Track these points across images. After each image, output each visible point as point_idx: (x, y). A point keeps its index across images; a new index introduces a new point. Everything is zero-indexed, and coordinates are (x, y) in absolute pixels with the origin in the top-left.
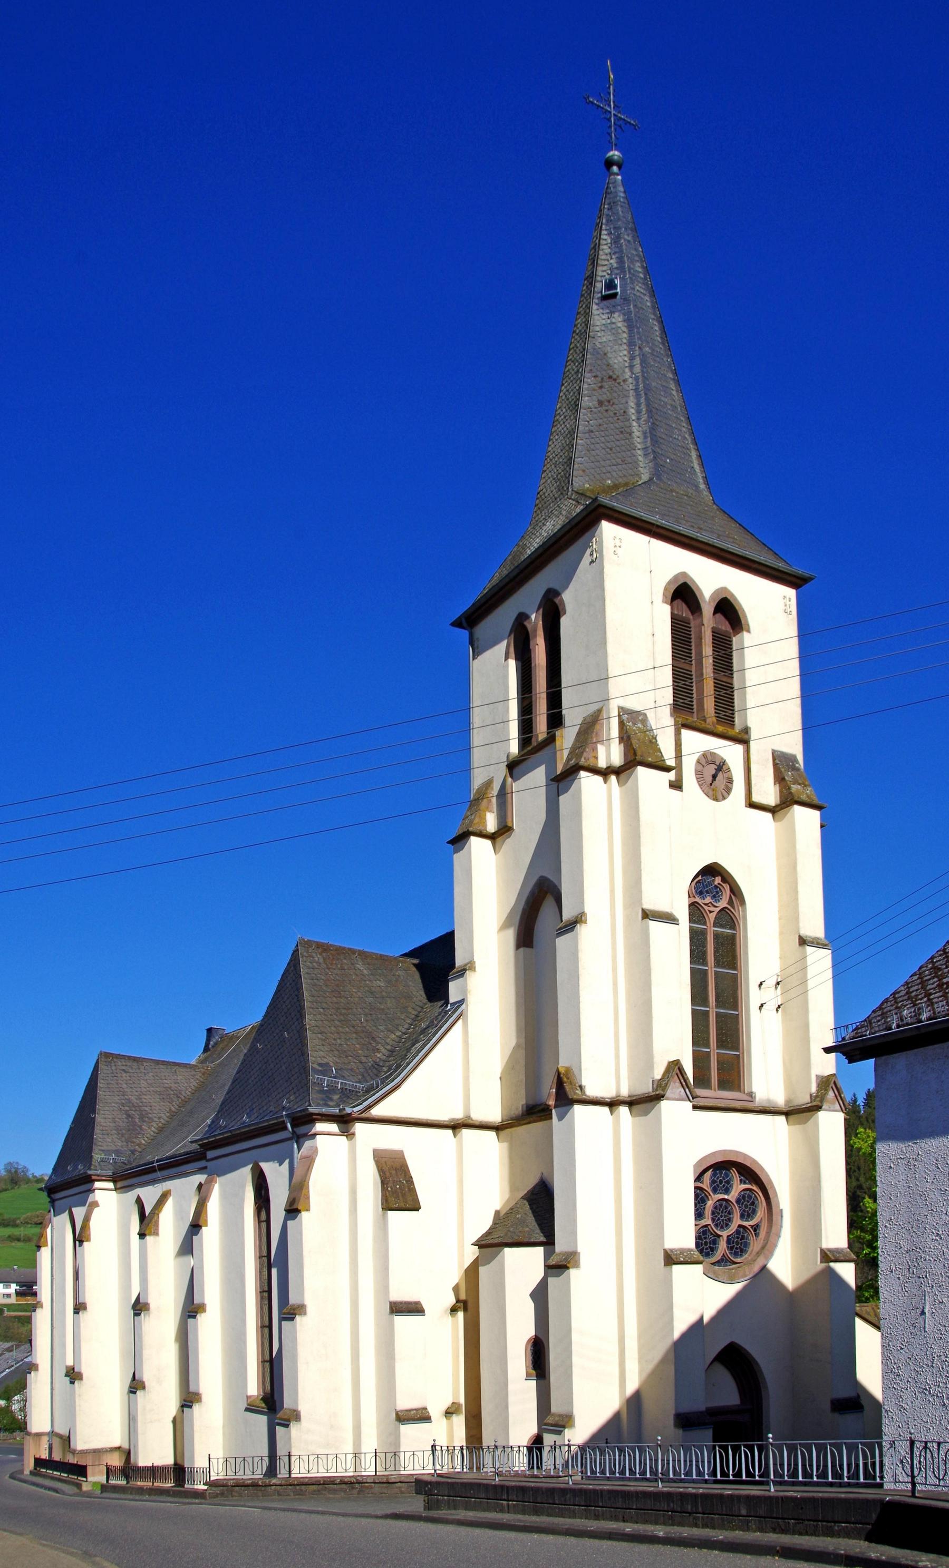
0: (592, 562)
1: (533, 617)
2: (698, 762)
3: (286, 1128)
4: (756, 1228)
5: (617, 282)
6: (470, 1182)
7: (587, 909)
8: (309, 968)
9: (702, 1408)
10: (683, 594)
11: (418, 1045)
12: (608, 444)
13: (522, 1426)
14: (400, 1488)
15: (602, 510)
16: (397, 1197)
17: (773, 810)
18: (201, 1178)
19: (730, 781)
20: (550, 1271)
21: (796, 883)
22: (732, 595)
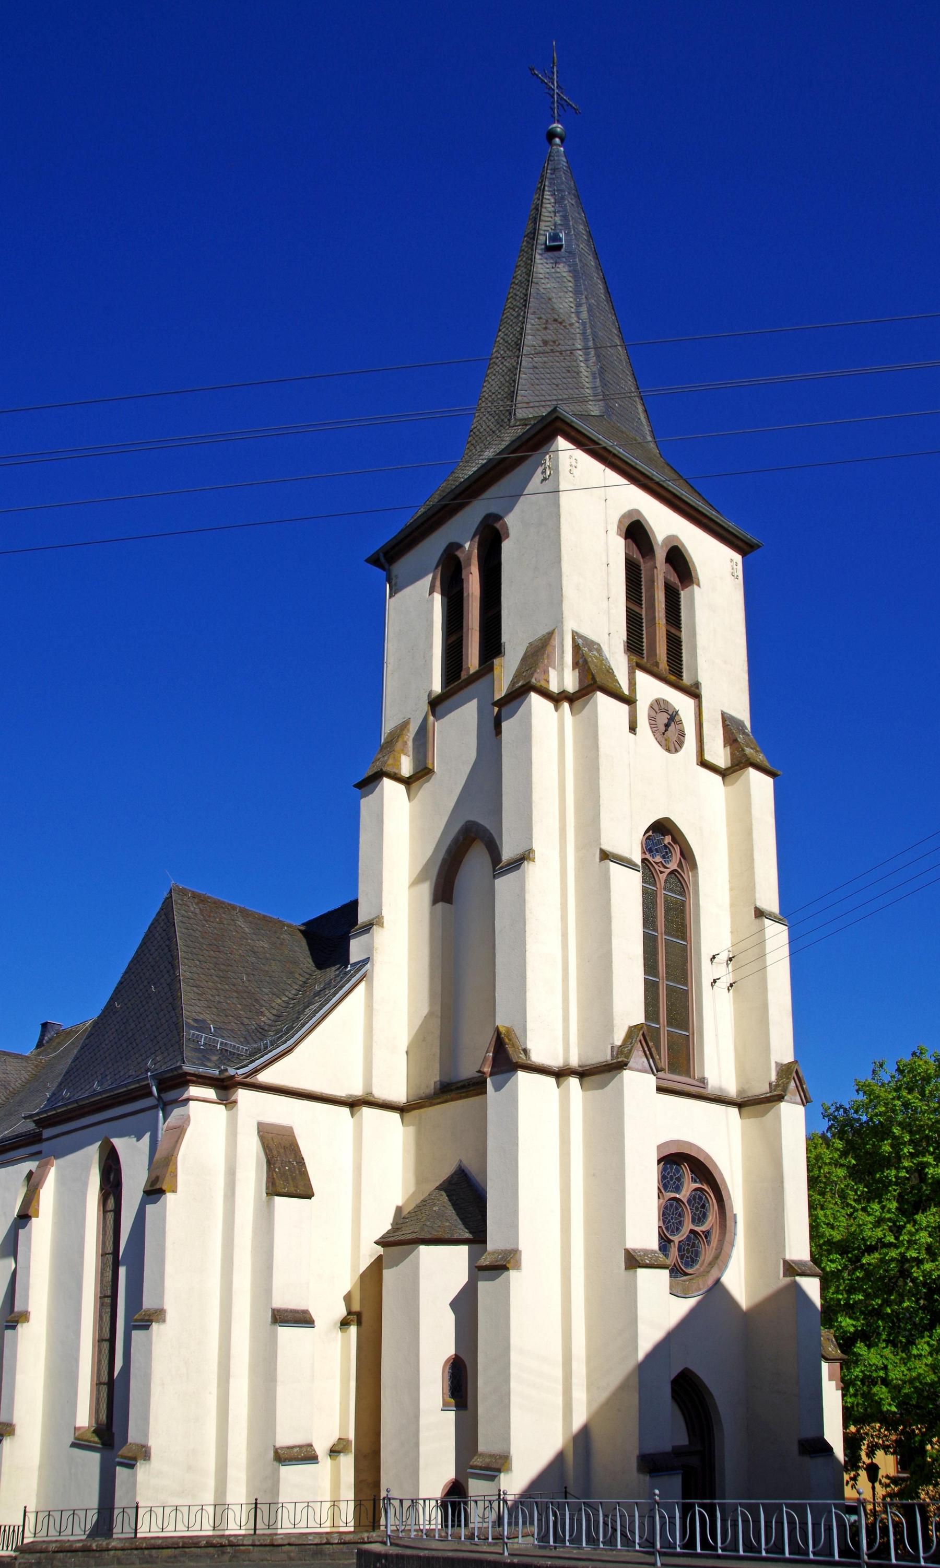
0: (545, 479)
1: (467, 545)
2: (651, 707)
3: (150, 1094)
4: (707, 1234)
5: (562, 235)
6: (370, 1171)
7: (535, 846)
8: (183, 916)
9: (668, 1448)
10: (636, 532)
11: (313, 1007)
12: (554, 381)
13: (436, 1469)
14: (288, 1552)
15: (559, 424)
16: (287, 1180)
17: (723, 773)
18: (31, 1165)
19: (682, 734)
20: (481, 1273)
21: (752, 850)
22: (683, 545)
